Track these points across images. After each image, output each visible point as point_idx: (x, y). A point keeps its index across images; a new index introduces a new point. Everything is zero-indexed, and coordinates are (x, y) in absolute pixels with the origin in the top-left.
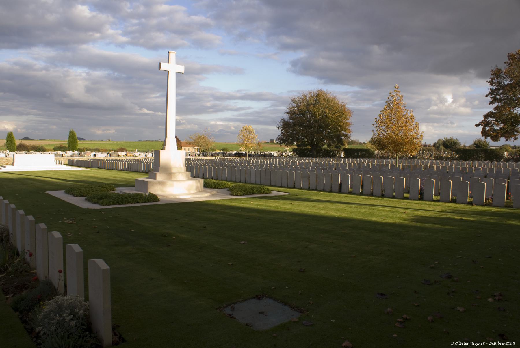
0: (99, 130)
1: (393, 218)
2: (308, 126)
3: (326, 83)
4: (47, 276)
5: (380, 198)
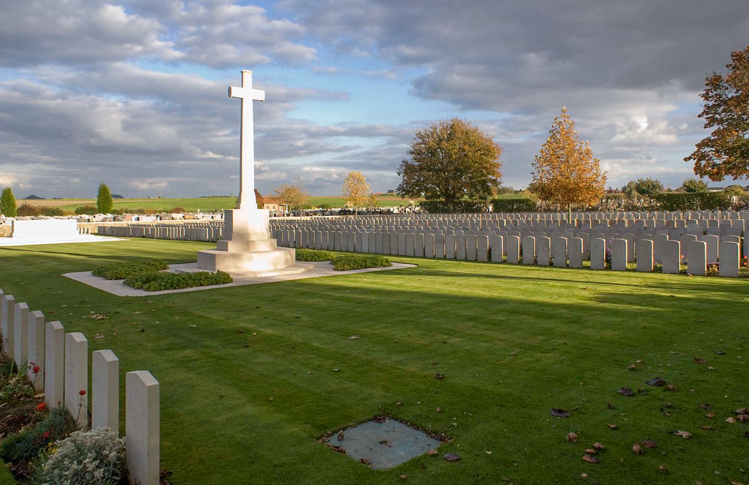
0: (143, 183)
1: (568, 296)
2: (441, 170)
3: (464, 109)
4: (62, 402)
5: (548, 269)
